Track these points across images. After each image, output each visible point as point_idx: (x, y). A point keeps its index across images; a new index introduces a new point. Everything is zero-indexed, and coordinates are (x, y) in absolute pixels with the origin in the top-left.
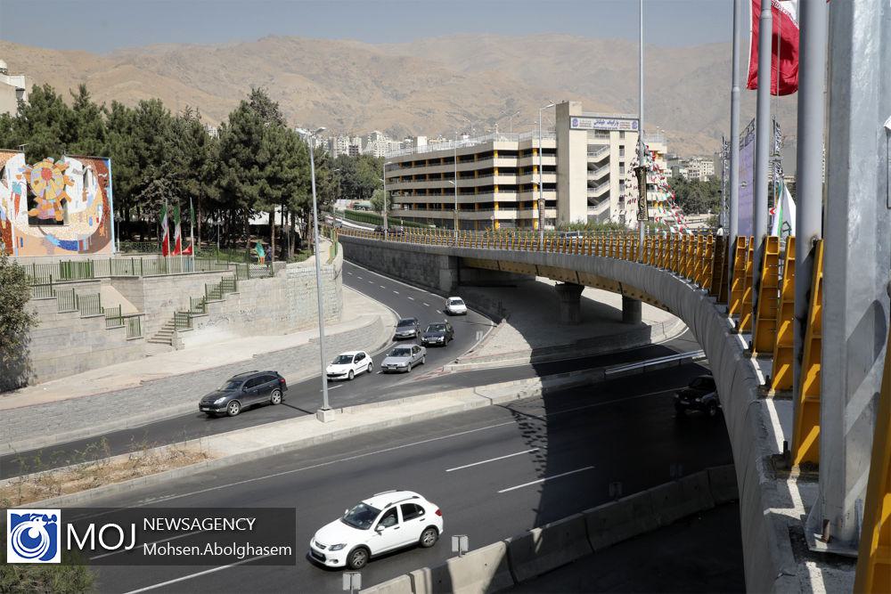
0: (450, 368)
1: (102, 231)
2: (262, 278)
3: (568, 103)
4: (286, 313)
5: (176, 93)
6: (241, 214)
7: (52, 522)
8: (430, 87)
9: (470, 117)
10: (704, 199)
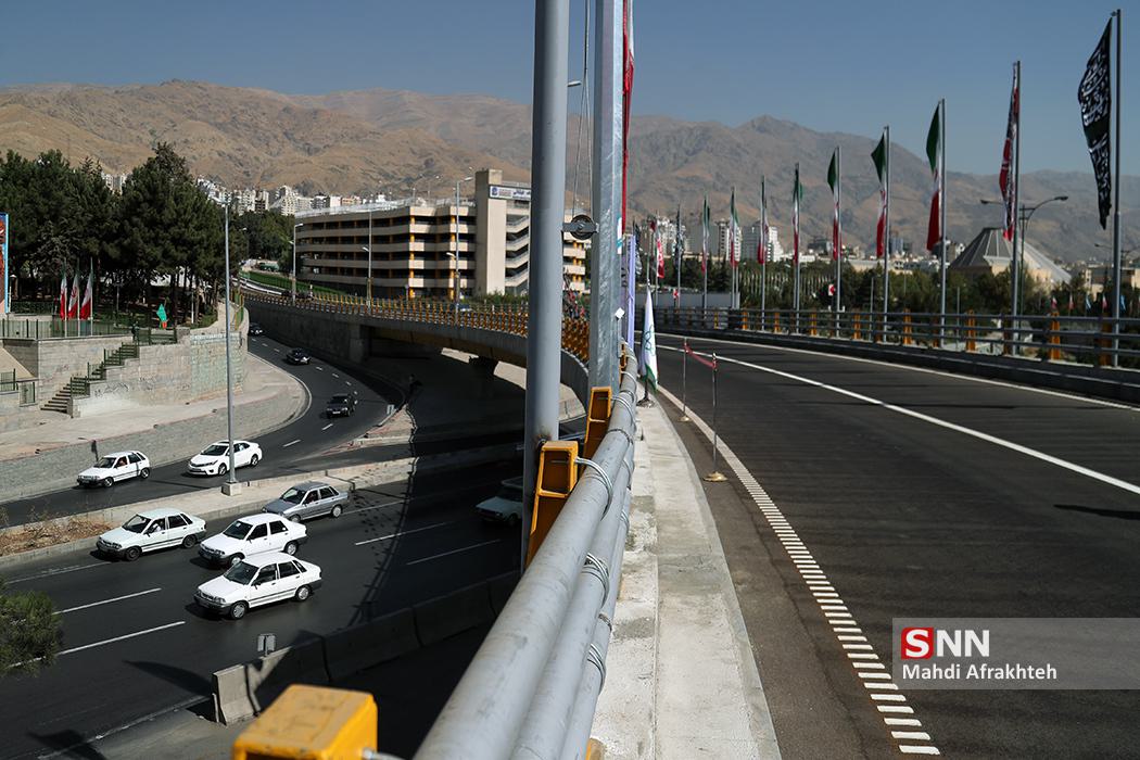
0: (360, 442)
2: (164, 344)
3: (487, 172)
4: (188, 381)
6: (141, 275)
9: (387, 176)
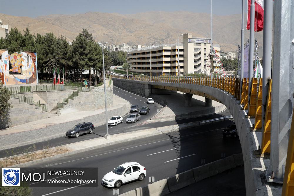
0: (149, 121)
1: (34, 76)
2: (86, 92)
3: (187, 34)
4: (94, 103)
5: (58, 31)
6: (79, 71)
7: (17, 172)
8: (142, 29)
9: (155, 38)
10: (232, 66)
